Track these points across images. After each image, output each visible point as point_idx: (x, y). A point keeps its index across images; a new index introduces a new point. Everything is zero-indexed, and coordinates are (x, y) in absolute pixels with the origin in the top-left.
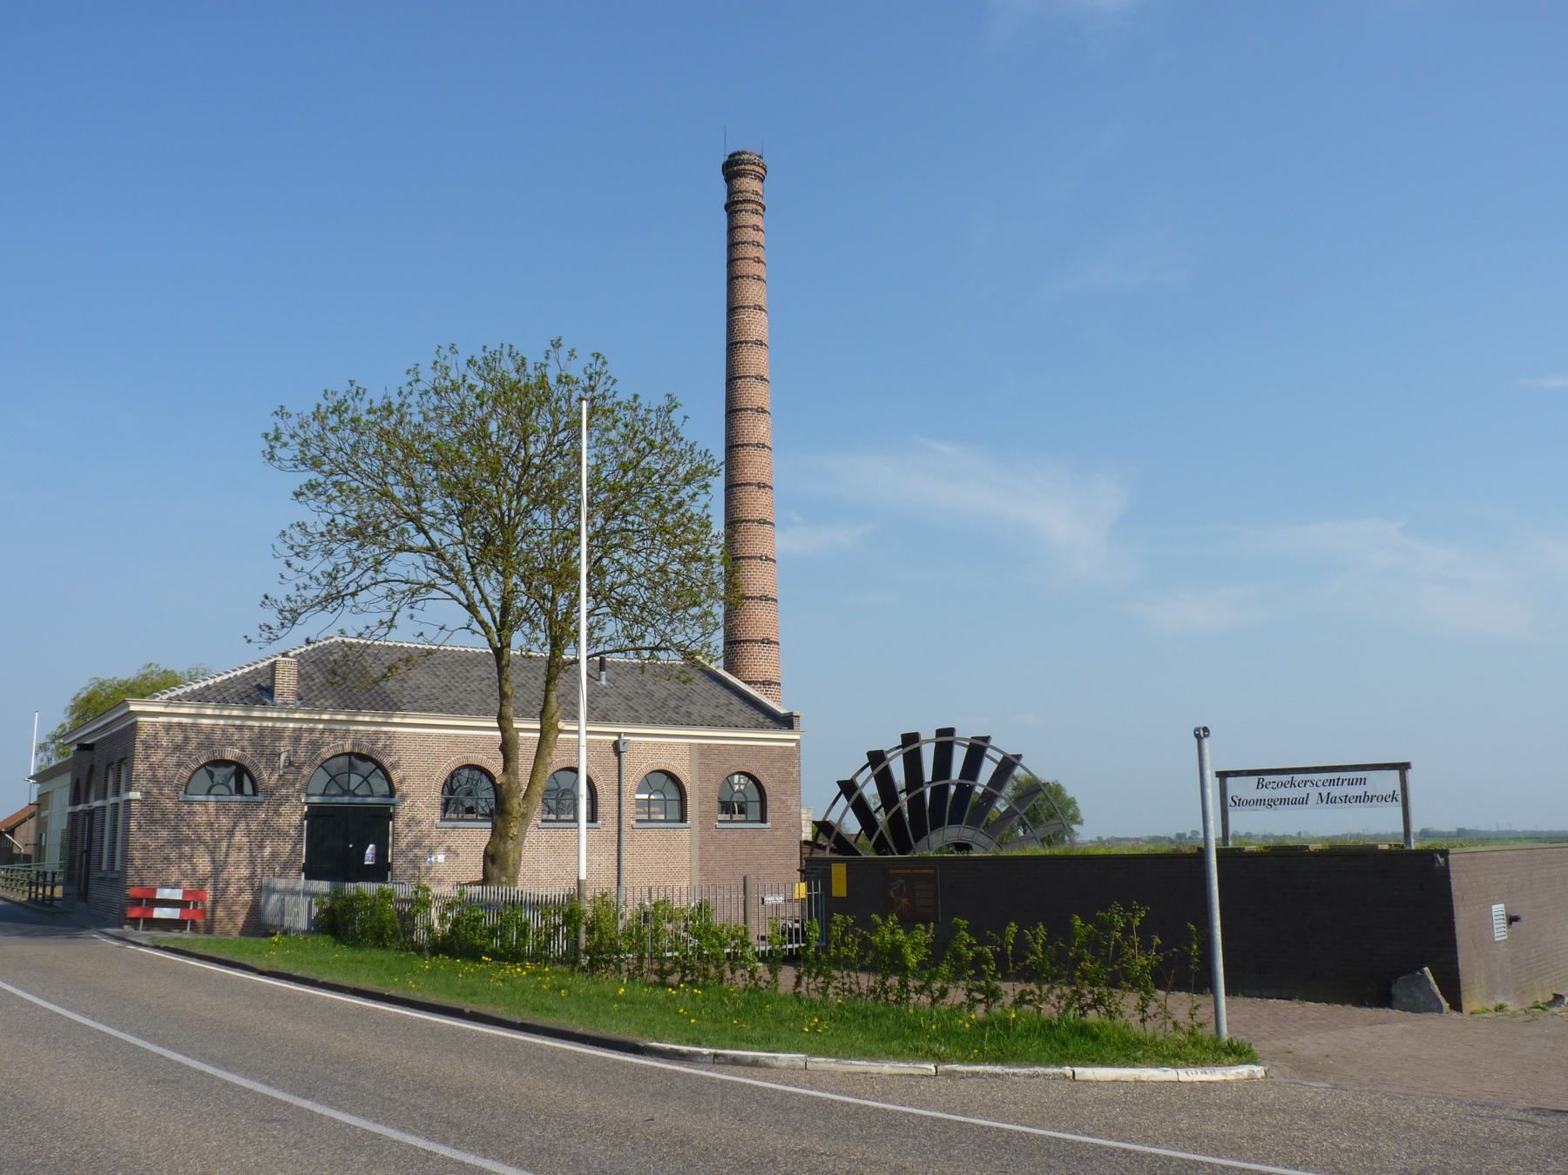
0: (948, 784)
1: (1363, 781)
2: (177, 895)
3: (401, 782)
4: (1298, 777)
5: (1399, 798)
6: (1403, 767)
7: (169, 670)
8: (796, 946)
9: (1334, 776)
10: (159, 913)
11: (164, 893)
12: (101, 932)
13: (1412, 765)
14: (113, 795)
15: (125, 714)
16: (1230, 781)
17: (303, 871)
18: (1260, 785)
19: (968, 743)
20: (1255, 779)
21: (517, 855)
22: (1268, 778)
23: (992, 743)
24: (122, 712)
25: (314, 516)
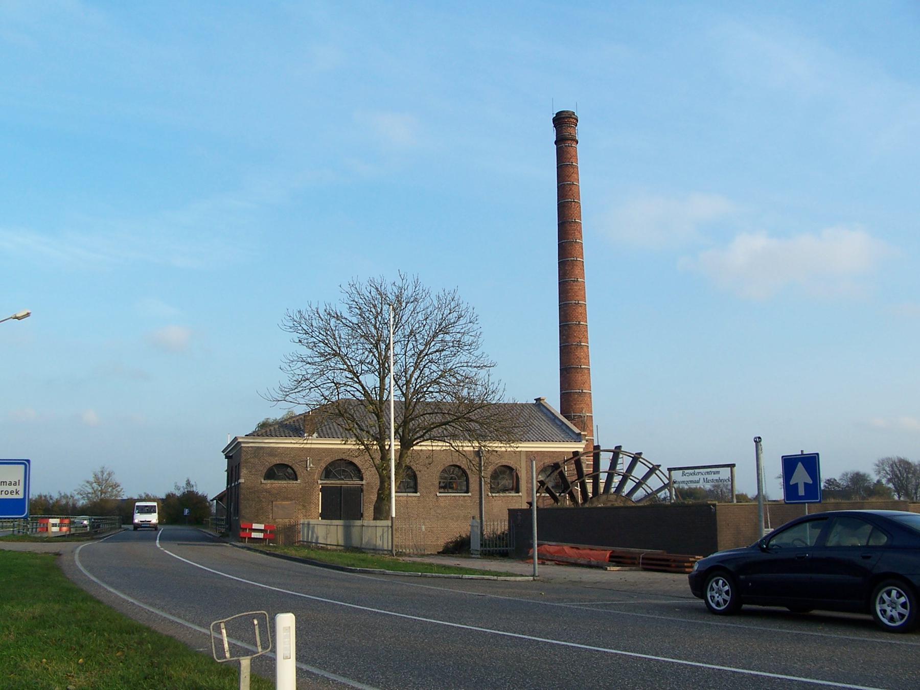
0: (613, 473)
1: (718, 472)
2: (262, 527)
3: (781, 488)
4: (697, 471)
5: (730, 480)
6: (26, 463)
7: (271, 421)
8: (492, 549)
9: (709, 470)
10: (254, 535)
11: (255, 526)
12: (199, 530)
13: (736, 465)
14: (765, 528)
15: (237, 443)
16: (673, 472)
17: (320, 516)
18: (684, 474)
19: (592, 454)
20: (681, 471)
21: (387, 507)
22: (686, 471)
23: (642, 456)
24: (236, 443)
25: (305, 352)
